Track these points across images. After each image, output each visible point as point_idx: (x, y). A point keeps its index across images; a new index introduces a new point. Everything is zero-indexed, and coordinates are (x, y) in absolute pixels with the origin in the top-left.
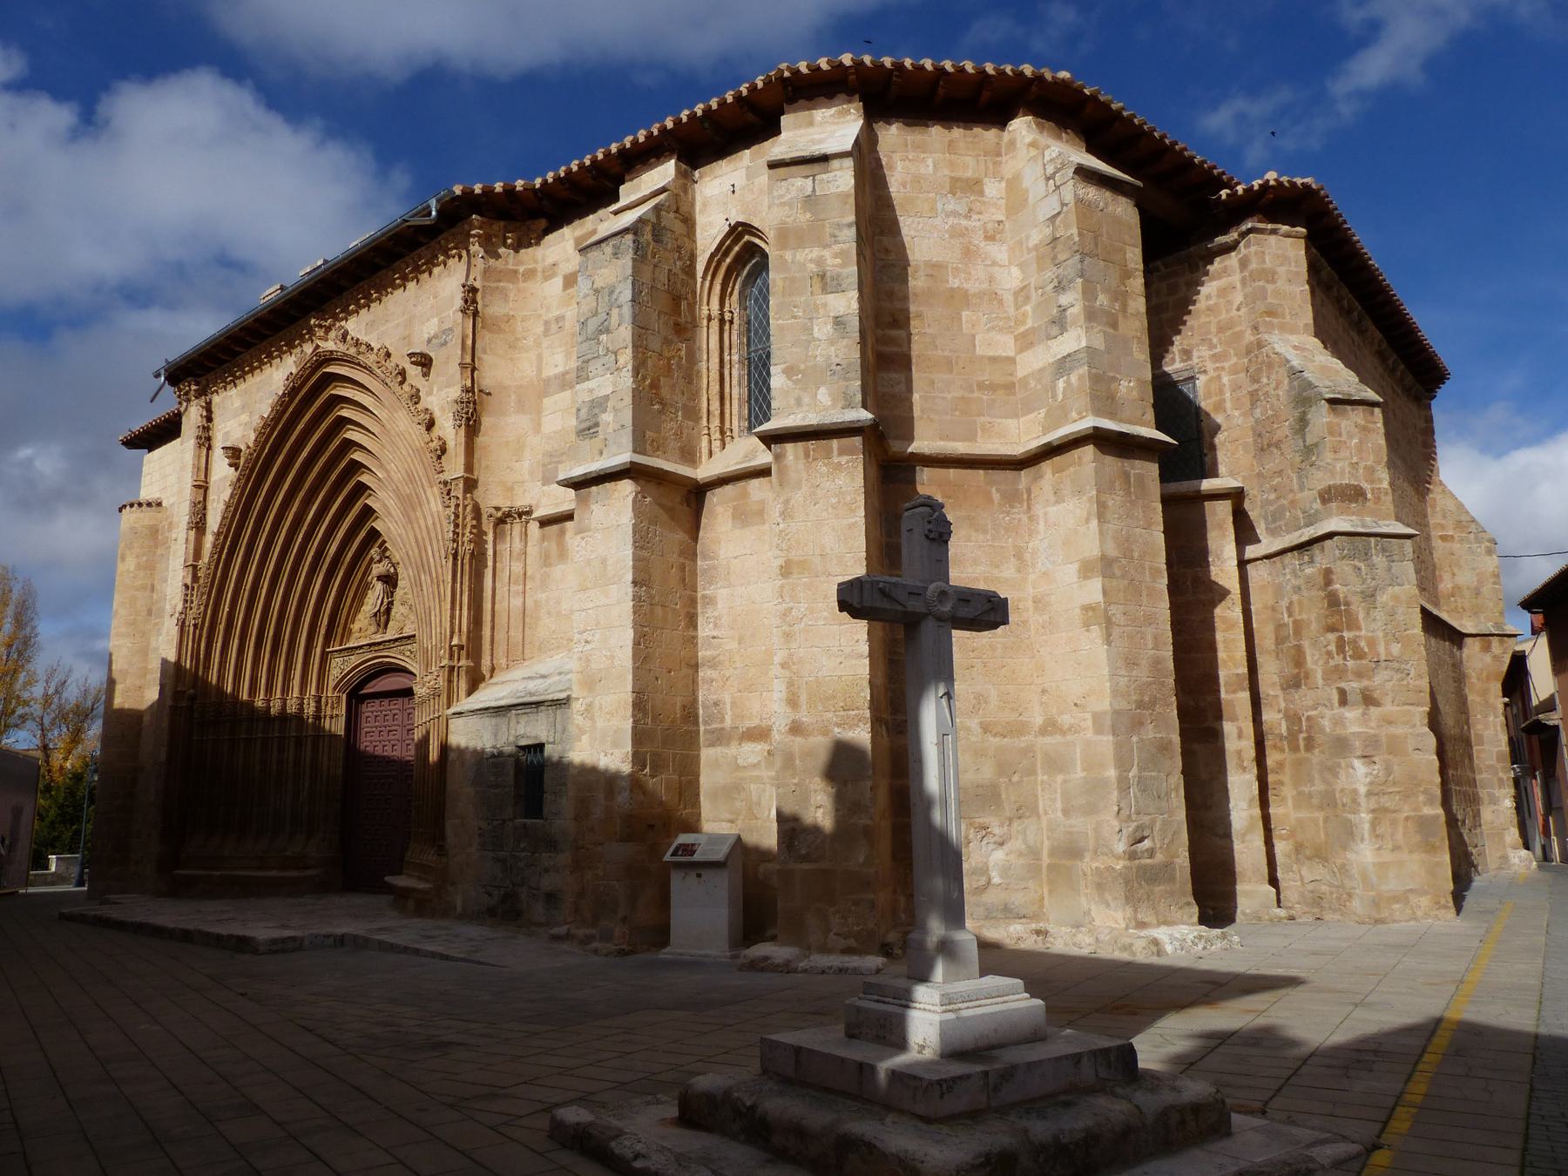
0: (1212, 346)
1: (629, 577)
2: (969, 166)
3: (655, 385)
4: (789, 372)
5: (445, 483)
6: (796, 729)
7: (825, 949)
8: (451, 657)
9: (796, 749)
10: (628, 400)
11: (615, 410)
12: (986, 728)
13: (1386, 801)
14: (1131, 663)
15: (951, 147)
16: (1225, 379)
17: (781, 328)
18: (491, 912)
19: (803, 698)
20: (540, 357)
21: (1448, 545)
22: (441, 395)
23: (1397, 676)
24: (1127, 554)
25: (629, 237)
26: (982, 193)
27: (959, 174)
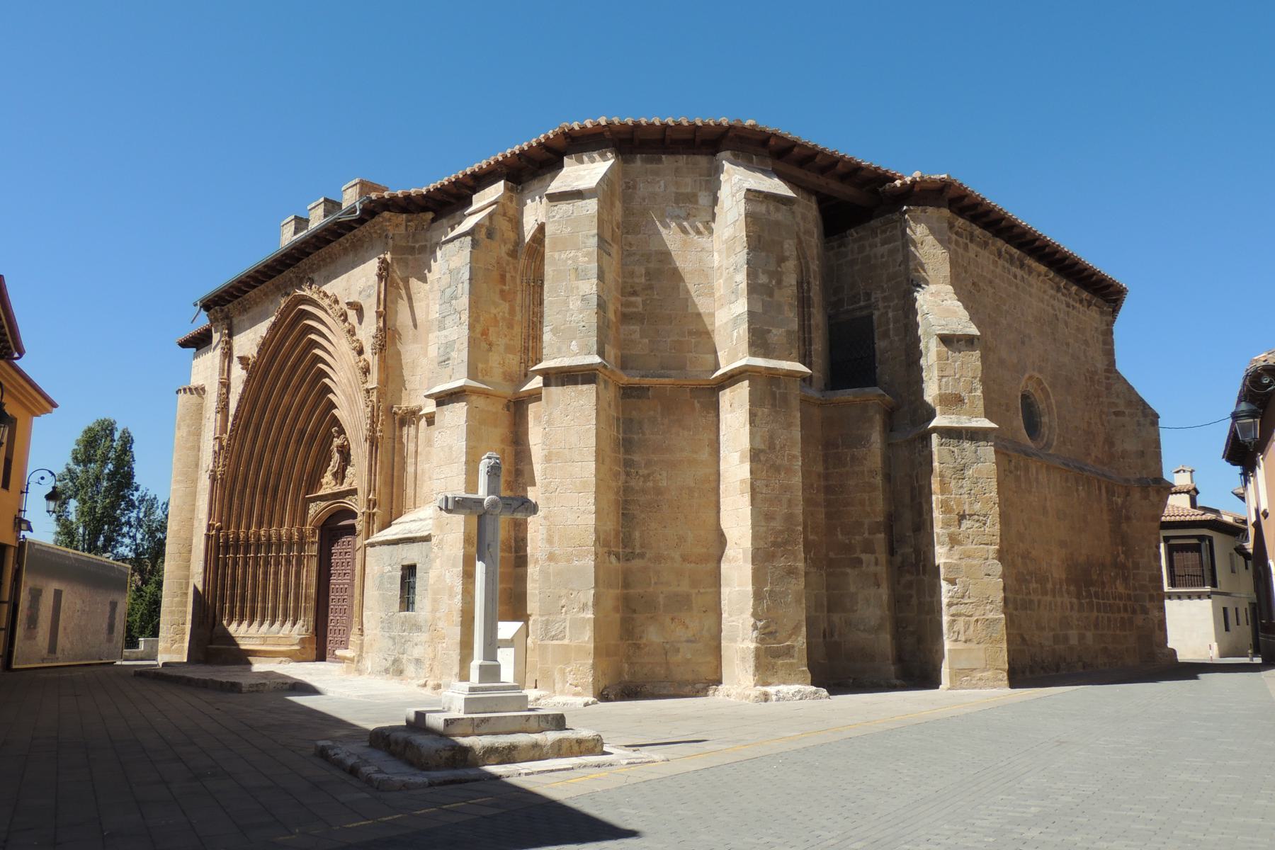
0: (883, 291)
1: (464, 459)
2: (688, 184)
3: (485, 333)
4: (555, 331)
5: (368, 391)
6: (551, 557)
7: (562, 693)
8: (369, 508)
9: (551, 570)
10: (466, 344)
11: (459, 350)
12: (685, 559)
13: (962, 609)
14: (769, 517)
15: (677, 171)
16: (890, 315)
17: (551, 302)
18: (387, 671)
19: (556, 539)
20: (428, 306)
21: (1120, 418)
22: (367, 331)
23: (977, 525)
24: (772, 447)
25: (469, 238)
26: (696, 202)
27: (683, 190)
